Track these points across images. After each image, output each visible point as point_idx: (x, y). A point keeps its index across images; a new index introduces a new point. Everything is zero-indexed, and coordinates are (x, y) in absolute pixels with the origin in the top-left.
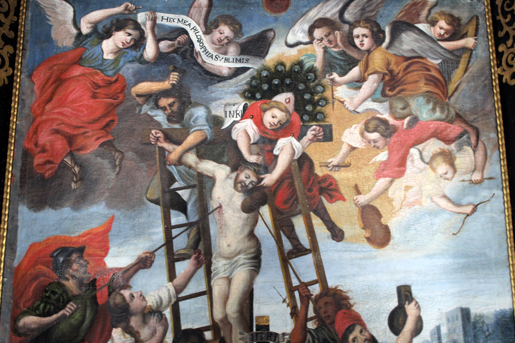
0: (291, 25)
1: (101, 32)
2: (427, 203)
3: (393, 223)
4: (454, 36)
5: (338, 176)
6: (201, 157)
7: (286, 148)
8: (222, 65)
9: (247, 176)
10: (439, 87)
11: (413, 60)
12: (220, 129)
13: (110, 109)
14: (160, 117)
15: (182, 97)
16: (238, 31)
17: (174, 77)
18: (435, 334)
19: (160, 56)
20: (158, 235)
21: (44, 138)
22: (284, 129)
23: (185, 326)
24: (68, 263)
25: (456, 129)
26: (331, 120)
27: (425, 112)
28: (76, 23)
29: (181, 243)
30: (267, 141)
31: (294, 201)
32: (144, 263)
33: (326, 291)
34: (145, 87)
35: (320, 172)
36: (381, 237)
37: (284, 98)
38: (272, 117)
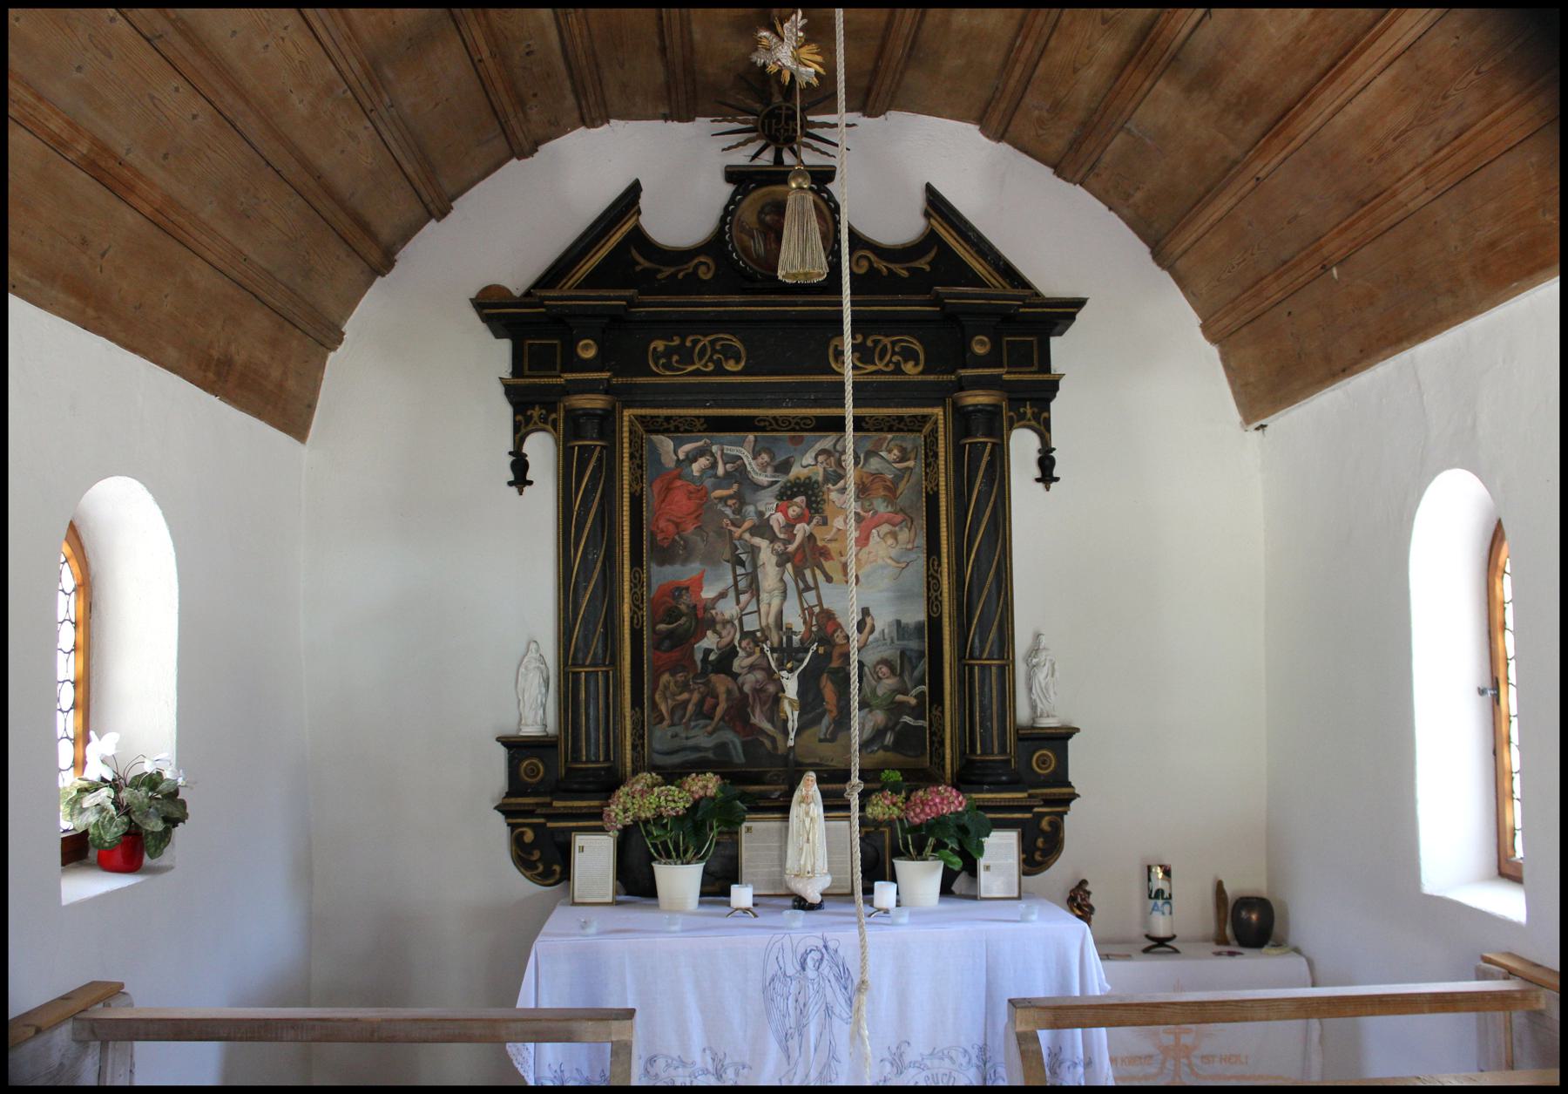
0: (803, 454)
1: (692, 458)
2: (880, 562)
4: (902, 459)
5: (832, 546)
6: (752, 535)
7: (801, 529)
8: (763, 479)
9: (779, 546)
10: (891, 492)
11: (877, 475)
14: (728, 511)
15: (741, 500)
16: (773, 458)
17: (735, 486)
18: (987, 868)
19: (727, 473)
20: (730, 581)
21: (662, 524)
22: (799, 518)
23: (746, 629)
24: (680, 596)
25: (899, 518)
26: (827, 513)
27: (882, 507)
28: (676, 453)
29: (742, 584)
30: (790, 526)
31: (808, 559)
32: (723, 595)
33: (823, 611)
35: (820, 543)
37: (800, 499)
38: (793, 511)
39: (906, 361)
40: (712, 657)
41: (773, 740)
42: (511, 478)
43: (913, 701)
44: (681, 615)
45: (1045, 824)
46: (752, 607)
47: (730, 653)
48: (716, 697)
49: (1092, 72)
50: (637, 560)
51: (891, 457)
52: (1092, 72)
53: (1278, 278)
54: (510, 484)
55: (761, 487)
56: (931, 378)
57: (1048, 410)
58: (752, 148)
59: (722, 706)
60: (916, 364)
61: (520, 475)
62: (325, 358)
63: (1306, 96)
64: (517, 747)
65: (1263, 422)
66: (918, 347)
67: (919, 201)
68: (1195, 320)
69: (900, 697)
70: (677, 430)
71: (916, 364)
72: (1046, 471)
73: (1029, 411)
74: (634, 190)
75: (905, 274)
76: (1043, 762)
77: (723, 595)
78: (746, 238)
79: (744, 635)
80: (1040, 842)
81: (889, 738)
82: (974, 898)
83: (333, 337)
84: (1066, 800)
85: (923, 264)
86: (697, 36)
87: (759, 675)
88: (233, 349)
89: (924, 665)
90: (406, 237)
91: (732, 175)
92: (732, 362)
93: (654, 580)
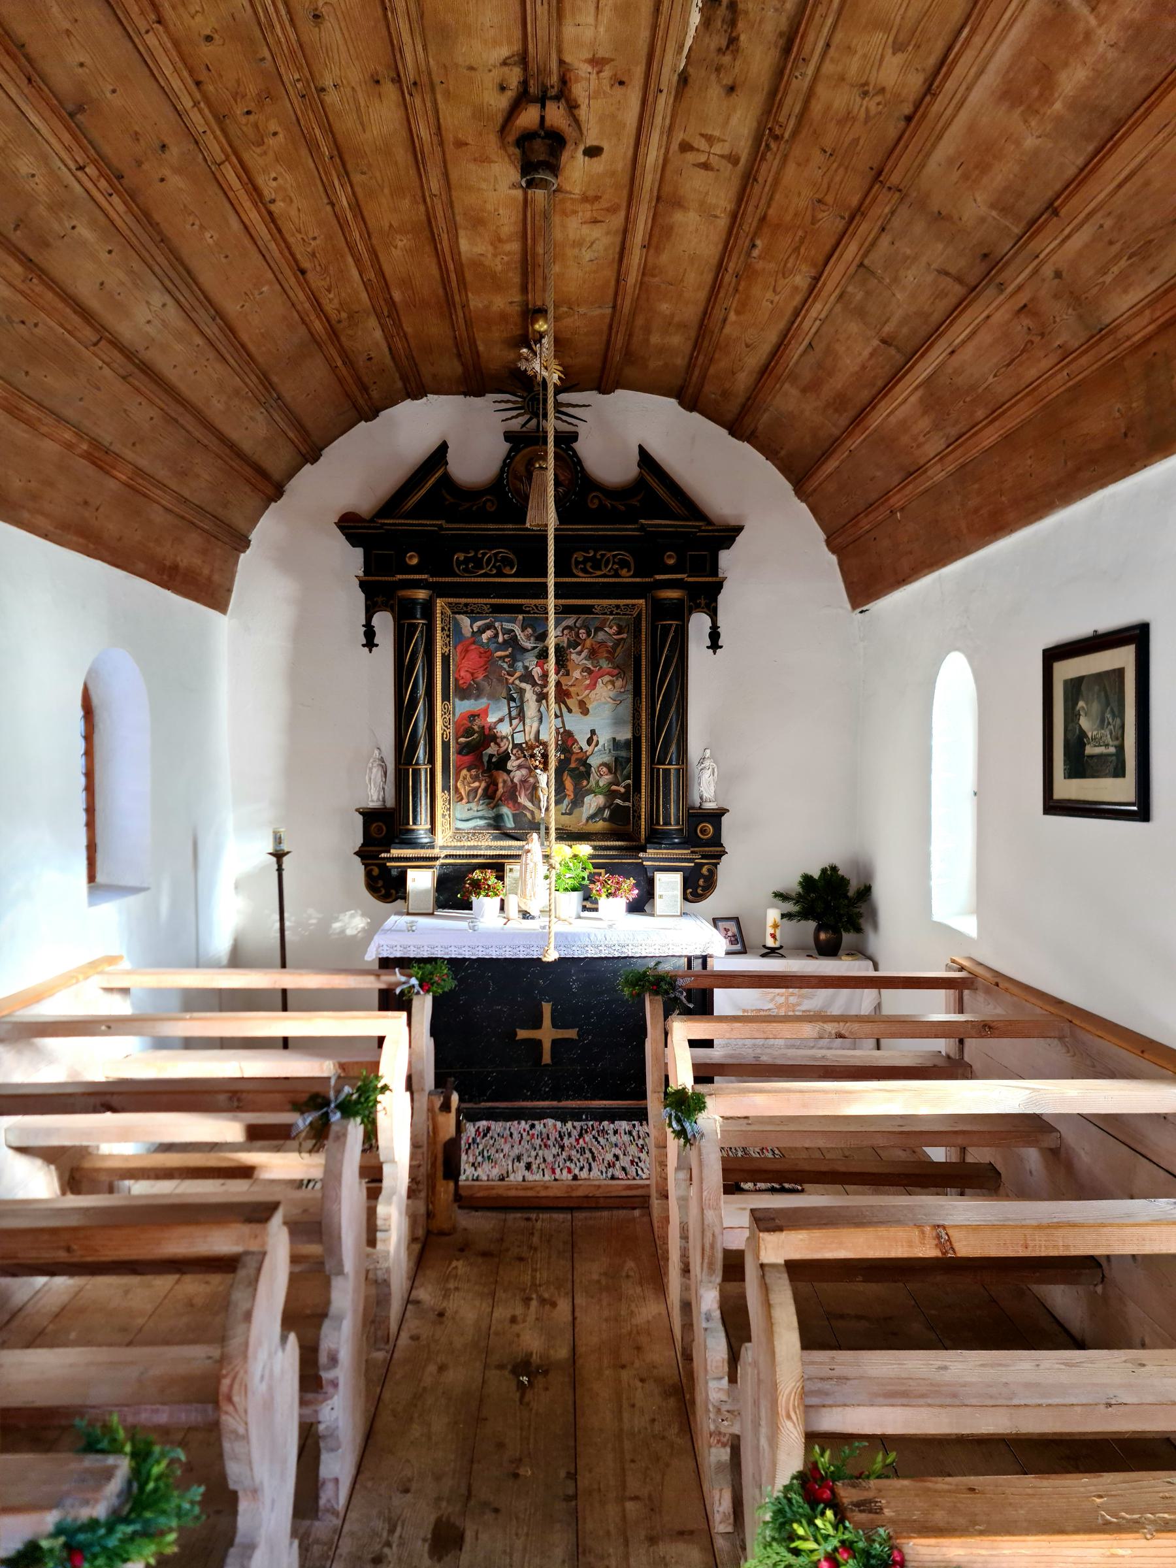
1: (482, 631)
3: (590, 707)
4: (619, 633)
5: (572, 689)
8: (528, 645)
9: (538, 689)
10: (611, 653)
12: (847, 897)
13: (486, 663)
14: (505, 666)
15: (514, 659)
16: (534, 631)
17: (510, 650)
19: (505, 641)
20: (507, 711)
21: (462, 674)
25: (616, 671)
26: (569, 668)
27: (605, 664)
29: (514, 713)
32: (501, 720)
34: (499, 654)
36: (585, 712)
39: (622, 568)
40: (494, 760)
41: (532, 813)
42: (364, 642)
43: (623, 790)
44: (474, 732)
45: (704, 871)
46: (520, 728)
47: (505, 757)
48: (497, 785)
49: (744, 374)
50: (446, 697)
51: (611, 631)
52: (744, 374)
53: (867, 516)
54: (364, 646)
55: (526, 650)
56: (638, 580)
57: (716, 601)
58: (522, 420)
59: (501, 790)
60: (629, 571)
61: (370, 641)
62: (238, 557)
63: (872, 404)
64: (370, 816)
65: (864, 608)
66: (630, 559)
67: (637, 450)
68: (822, 536)
69: (614, 787)
70: (472, 612)
71: (629, 571)
72: (715, 642)
73: (703, 602)
74: (443, 448)
75: (623, 508)
76: (703, 831)
77: (501, 720)
78: (518, 483)
79: (515, 746)
80: (701, 882)
81: (607, 813)
82: (653, 915)
83: (243, 543)
84: (719, 856)
85: (635, 502)
86: (481, 348)
87: (524, 772)
88: (179, 559)
89: (630, 767)
90: (290, 476)
91: (509, 436)
92: (508, 568)
93: (457, 710)
